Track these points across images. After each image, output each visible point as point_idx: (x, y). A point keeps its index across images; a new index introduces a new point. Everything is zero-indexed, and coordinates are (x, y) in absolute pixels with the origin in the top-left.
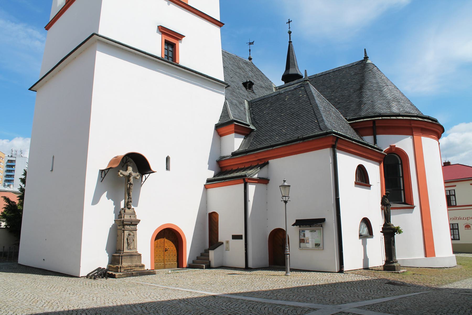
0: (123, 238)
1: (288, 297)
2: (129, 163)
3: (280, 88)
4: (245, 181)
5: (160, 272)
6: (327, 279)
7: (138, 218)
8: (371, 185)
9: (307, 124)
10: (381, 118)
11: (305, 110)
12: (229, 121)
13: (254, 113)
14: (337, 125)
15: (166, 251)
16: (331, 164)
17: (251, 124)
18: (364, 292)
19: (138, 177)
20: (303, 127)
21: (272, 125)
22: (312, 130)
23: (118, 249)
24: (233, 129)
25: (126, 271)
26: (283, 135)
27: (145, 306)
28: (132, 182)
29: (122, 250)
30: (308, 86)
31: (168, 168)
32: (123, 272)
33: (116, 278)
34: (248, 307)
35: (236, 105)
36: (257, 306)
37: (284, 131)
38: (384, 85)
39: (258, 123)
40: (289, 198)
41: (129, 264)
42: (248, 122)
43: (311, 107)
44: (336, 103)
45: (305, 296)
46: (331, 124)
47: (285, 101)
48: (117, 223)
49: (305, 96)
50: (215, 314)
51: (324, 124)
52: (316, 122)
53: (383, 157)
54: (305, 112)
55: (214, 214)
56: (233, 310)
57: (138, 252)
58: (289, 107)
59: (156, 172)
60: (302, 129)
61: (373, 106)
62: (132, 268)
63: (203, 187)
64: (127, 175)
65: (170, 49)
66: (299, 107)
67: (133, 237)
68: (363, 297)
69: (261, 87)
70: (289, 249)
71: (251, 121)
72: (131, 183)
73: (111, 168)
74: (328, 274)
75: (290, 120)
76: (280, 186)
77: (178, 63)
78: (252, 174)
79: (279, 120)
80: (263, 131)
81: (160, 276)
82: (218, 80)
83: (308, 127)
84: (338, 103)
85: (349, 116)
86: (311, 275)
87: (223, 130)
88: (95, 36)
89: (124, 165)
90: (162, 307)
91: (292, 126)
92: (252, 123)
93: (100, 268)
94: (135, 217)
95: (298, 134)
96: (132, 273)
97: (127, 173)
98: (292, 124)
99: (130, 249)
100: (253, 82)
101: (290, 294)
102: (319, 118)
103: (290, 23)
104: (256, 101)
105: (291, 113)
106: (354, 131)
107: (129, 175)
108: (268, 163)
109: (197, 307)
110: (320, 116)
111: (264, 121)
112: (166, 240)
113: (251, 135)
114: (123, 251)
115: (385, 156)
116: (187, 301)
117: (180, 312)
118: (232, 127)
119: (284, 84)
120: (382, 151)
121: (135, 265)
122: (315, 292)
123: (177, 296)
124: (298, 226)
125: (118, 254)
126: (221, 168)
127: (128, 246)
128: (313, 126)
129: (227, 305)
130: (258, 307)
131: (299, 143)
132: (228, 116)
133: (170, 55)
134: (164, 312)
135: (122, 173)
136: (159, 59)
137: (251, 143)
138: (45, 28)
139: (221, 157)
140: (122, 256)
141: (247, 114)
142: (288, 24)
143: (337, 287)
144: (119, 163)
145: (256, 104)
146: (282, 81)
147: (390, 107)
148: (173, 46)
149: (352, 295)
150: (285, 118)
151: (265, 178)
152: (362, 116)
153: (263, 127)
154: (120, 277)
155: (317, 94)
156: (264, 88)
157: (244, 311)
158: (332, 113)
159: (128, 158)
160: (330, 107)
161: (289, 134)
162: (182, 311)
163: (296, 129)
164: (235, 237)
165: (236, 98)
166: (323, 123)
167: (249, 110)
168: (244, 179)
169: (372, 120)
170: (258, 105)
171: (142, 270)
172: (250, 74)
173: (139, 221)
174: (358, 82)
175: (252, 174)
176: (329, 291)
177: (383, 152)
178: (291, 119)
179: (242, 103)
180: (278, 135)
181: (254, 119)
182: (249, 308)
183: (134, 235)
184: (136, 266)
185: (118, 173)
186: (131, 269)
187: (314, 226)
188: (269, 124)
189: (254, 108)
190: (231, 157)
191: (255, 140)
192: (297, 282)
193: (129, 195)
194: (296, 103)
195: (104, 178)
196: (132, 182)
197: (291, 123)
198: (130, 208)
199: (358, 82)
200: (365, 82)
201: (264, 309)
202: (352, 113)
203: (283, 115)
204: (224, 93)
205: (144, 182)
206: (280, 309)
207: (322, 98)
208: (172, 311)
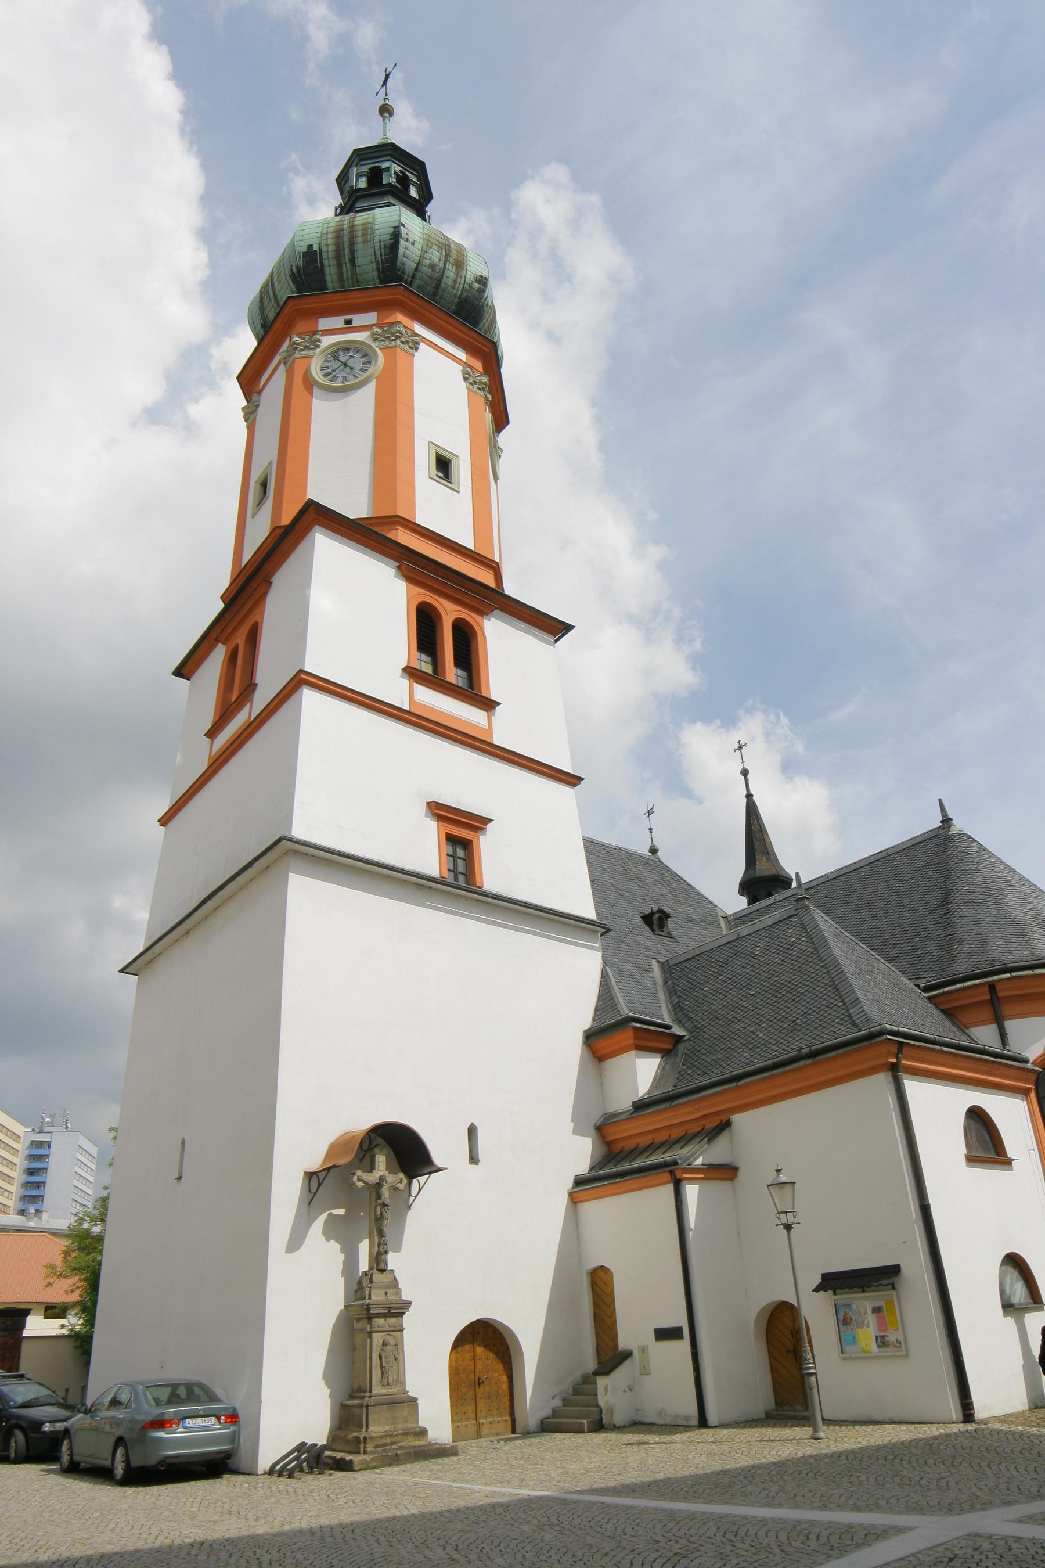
0: (368, 1355)
1: (825, 1499)
2: (376, 1150)
3: (739, 919)
4: (675, 1176)
5: (472, 1447)
6: (930, 1442)
7: (405, 1296)
8: (1013, 1160)
9: (818, 1013)
10: (1008, 975)
11: (809, 976)
12: (618, 1021)
13: (678, 993)
14: (896, 1007)
15: (479, 1384)
16: (893, 1112)
17: (674, 1021)
18: (1037, 1477)
19: (401, 1186)
20: (809, 1022)
21: (730, 1020)
22: (832, 1029)
23: (355, 1388)
24: (631, 1041)
25: (379, 1449)
26: (759, 1045)
27: (454, 1544)
28: (387, 1202)
29: (368, 1389)
30: (809, 914)
31: (473, 1159)
32: (373, 1452)
33: (355, 1471)
34: (722, 1533)
35: (631, 976)
36: (745, 1529)
37: (761, 1035)
38: (1003, 886)
39: (692, 1018)
40: (795, 1217)
41: (387, 1428)
42: (667, 1020)
43: (822, 966)
44: (885, 945)
45: (873, 1496)
46: (878, 1008)
47: (753, 957)
48: (351, 1313)
49: (804, 939)
50: (639, 1554)
51: (861, 1010)
52: (839, 1007)
53: (1034, 1077)
54: (808, 981)
55: (601, 1273)
56: (683, 1541)
57: (408, 1392)
58: (767, 972)
59: (446, 1169)
60: (807, 1028)
61: (983, 947)
62: (394, 1439)
63: (564, 1198)
64: (375, 1182)
65: (460, 853)
66: (792, 969)
67: (395, 1351)
68: (1034, 1489)
69: (690, 920)
70: (814, 1360)
71: (675, 1014)
72: (383, 1203)
73: (334, 1167)
74: (932, 1429)
75: (775, 1006)
76: (768, 1186)
77: (481, 888)
78: (691, 1156)
79: (746, 1007)
80: (708, 1040)
81: (470, 1459)
82: (580, 918)
83: (821, 1020)
84: (890, 944)
85: (924, 978)
86: (885, 1434)
87: (604, 1044)
88: (284, 842)
89: (365, 1155)
90: (496, 1543)
91: (779, 1020)
92: (677, 1019)
93: (303, 1444)
94: (399, 1292)
95: (797, 1041)
96: (397, 1454)
97: (372, 1178)
98: (780, 1017)
99: (388, 1384)
100: (667, 910)
101: (831, 1492)
102: (846, 995)
104: (681, 960)
105: (774, 988)
106: (942, 1016)
107: (378, 1181)
108: (728, 1124)
109: (588, 1538)
110: (849, 989)
111: (707, 1011)
112: (479, 1350)
113: (678, 1051)
114: (371, 1391)
115: (1036, 1075)
116: (558, 1525)
117: (547, 1555)
118: (626, 1036)
119: (746, 906)
120: (1026, 1061)
121: (403, 1430)
122: (900, 1481)
123: (529, 1513)
124: (830, 1292)
125: (356, 1402)
126: (608, 1144)
127: (382, 1377)
128: (835, 1018)
129: (667, 1529)
130: (748, 1530)
131: (805, 1066)
132: (614, 1006)
133: (461, 867)
134: (506, 1556)
135: (363, 1178)
136: (437, 883)
137: (679, 1073)
138: (158, 821)
139: (606, 1114)
140: (367, 1406)
141: (662, 996)
143: (961, 1463)
144: (354, 1152)
145: (683, 969)
147: (1027, 944)
148: (466, 845)
149: (1003, 1486)
150: (759, 1000)
151: (726, 1165)
152: (958, 976)
153: (705, 1027)
154: (366, 1467)
155: (833, 931)
156: (697, 922)
157: (713, 1544)
158: (880, 977)
159: (375, 1138)
160: (871, 962)
161: (775, 1042)
162: (552, 1553)
163: (793, 1029)
164: (665, 1334)
165: (630, 956)
166: (859, 1006)
167: (664, 985)
168: (672, 1172)
169: (986, 983)
170: (688, 970)
171: (422, 1443)
172: (658, 889)
173: (408, 1304)
174: (935, 886)
175: (691, 1156)
176: (938, 1476)
177: (1029, 1066)
178: (775, 1001)
179: (646, 970)
180: (747, 1047)
181: (682, 1009)
182: (725, 1533)
183: (396, 1345)
184: (406, 1433)
185: (352, 1179)
186: (393, 1443)
187: (872, 1288)
188: (721, 1020)
189: (677, 980)
190: (631, 1114)
191: (689, 1065)
192: (847, 1457)
193: (381, 1233)
194: (783, 961)
195: (315, 1194)
196: (388, 1201)
197: (777, 1013)
198: (384, 1270)
199: (935, 886)
200: (952, 883)
201: (767, 1534)
202: (930, 968)
203: (754, 992)
204: (597, 945)
205: (416, 1196)
206: (807, 1532)
207: (847, 940)
208: (525, 1553)
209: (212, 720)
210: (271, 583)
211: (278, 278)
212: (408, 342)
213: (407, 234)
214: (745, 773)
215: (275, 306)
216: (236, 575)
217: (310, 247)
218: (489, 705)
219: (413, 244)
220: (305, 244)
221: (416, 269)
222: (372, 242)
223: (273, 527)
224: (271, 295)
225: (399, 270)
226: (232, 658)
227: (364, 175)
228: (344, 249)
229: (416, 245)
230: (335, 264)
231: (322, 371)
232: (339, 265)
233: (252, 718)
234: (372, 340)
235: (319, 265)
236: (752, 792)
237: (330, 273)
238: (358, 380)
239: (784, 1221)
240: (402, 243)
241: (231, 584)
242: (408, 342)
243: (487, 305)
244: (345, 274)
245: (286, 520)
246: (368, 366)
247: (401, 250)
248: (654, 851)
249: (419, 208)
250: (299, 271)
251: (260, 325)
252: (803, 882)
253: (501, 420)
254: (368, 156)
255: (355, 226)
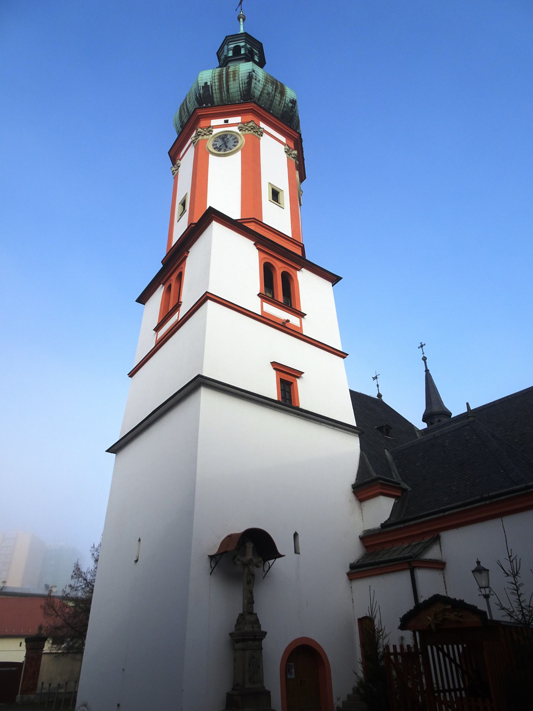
59: (285, 556)
73: (226, 552)
77: (299, 407)
94: (259, 626)
103: (423, 348)
142: (421, 349)
146: (423, 422)
209: (157, 322)
210: (189, 252)
211: (189, 100)
212: (257, 132)
213: (256, 76)
214: (424, 359)
215: (188, 115)
216: (159, 322)
217: (206, 83)
218: (301, 315)
219: (259, 81)
220: (204, 81)
221: (261, 95)
222: (238, 80)
223: (190, 224)
224: (186, 110)
225: (251, 95)
226: (169, 289)
227: (231, 50)
228: (223, 84)
229: (261, 82)
230: (219, 92)
231: (213, 146)
232: (221, 93)
233: (179, 319)
234: (239, 130)
235: (211, 93)
236: (429, 368)
237: (216, 96)
238: (231, 151)
239: (484, 593)
240: (254, 81)
241: (167, 255)
242: (257, 132)
243: (296, 116)
244: (224, 98)
245: (196, 220)
246: (237, 143)
247: (253, 85)
248: (379, 395)
249: (262, 64)
250: (200, 96)
251: (180, 126)
252: (472, 409)
253: (303, 177)
254: (236, 39)
255: (229, 72)
